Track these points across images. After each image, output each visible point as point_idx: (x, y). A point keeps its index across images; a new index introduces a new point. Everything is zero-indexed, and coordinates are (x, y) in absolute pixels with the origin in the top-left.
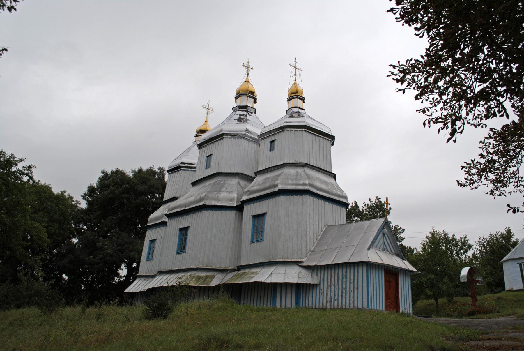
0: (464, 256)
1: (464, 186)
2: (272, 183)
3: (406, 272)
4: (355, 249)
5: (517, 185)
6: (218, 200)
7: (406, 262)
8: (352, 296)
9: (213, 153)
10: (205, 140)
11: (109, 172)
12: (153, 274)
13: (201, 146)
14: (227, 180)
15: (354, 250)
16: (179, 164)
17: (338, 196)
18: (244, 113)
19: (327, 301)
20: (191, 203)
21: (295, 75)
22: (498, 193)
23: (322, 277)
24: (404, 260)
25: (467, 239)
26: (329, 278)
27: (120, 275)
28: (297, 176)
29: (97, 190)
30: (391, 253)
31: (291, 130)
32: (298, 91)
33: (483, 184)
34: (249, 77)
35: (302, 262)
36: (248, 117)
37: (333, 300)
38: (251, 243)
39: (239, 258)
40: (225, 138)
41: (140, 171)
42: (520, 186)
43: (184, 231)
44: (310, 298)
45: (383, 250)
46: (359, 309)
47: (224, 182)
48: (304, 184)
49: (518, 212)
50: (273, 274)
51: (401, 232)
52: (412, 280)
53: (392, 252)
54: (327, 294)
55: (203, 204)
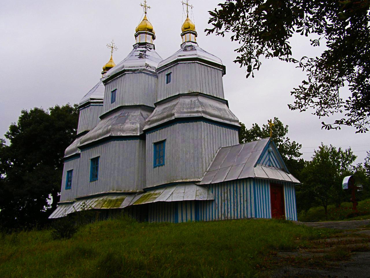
0: (349, 166)
1: (294, 109)
2: (169, 113)
3: (291, 184)
4: (243, 168)
5: (338, 106)
6: (123, 131)
7: (290, 175)
8: (242, 208)
9: (117, 88)
10: (110, 77)
11: (61, 107)
12: (72, 201)
13: (106, 82)
14: (131, 112)
15: (242, 168)
16: (88, 100)
17: (230, 120)
18: (144, 49)
19: (222, 214)
20: (100, 135)
21: (187, 11)
22: (322, 113)
23: (217, 194)
24: (289, 173)
25: (351, 151)
26: (223, 194)
27: (48, 204)
28: (191, 104)
29: (19, 128)
30: (277, 168)
31: (184, 63)
32: (191, 26)
33: (310, 107)
34: (147, 16)
35: (199, 182)
36: (148, 53)
37: (226, 213)
38: (154, 168)
39: (145, 181)
40: (127, 73)
41: (57, 108)
42: (340, 107)
43: (95, 161)
44: (208, 213)
45: (269, 166)
46: (248, 219)
47: (128, 115)
48: (198, 112)
49: (331, 129)
50: (173, 194)
51: (299, 147)
52: (296, 190)
53: (277, 167)
54: (221, 208)
55: (110, 136)
